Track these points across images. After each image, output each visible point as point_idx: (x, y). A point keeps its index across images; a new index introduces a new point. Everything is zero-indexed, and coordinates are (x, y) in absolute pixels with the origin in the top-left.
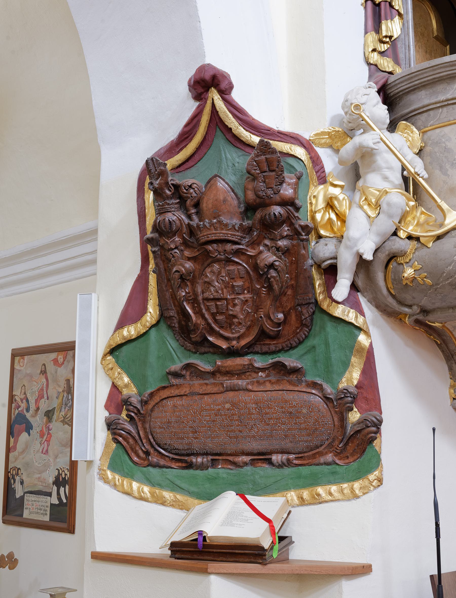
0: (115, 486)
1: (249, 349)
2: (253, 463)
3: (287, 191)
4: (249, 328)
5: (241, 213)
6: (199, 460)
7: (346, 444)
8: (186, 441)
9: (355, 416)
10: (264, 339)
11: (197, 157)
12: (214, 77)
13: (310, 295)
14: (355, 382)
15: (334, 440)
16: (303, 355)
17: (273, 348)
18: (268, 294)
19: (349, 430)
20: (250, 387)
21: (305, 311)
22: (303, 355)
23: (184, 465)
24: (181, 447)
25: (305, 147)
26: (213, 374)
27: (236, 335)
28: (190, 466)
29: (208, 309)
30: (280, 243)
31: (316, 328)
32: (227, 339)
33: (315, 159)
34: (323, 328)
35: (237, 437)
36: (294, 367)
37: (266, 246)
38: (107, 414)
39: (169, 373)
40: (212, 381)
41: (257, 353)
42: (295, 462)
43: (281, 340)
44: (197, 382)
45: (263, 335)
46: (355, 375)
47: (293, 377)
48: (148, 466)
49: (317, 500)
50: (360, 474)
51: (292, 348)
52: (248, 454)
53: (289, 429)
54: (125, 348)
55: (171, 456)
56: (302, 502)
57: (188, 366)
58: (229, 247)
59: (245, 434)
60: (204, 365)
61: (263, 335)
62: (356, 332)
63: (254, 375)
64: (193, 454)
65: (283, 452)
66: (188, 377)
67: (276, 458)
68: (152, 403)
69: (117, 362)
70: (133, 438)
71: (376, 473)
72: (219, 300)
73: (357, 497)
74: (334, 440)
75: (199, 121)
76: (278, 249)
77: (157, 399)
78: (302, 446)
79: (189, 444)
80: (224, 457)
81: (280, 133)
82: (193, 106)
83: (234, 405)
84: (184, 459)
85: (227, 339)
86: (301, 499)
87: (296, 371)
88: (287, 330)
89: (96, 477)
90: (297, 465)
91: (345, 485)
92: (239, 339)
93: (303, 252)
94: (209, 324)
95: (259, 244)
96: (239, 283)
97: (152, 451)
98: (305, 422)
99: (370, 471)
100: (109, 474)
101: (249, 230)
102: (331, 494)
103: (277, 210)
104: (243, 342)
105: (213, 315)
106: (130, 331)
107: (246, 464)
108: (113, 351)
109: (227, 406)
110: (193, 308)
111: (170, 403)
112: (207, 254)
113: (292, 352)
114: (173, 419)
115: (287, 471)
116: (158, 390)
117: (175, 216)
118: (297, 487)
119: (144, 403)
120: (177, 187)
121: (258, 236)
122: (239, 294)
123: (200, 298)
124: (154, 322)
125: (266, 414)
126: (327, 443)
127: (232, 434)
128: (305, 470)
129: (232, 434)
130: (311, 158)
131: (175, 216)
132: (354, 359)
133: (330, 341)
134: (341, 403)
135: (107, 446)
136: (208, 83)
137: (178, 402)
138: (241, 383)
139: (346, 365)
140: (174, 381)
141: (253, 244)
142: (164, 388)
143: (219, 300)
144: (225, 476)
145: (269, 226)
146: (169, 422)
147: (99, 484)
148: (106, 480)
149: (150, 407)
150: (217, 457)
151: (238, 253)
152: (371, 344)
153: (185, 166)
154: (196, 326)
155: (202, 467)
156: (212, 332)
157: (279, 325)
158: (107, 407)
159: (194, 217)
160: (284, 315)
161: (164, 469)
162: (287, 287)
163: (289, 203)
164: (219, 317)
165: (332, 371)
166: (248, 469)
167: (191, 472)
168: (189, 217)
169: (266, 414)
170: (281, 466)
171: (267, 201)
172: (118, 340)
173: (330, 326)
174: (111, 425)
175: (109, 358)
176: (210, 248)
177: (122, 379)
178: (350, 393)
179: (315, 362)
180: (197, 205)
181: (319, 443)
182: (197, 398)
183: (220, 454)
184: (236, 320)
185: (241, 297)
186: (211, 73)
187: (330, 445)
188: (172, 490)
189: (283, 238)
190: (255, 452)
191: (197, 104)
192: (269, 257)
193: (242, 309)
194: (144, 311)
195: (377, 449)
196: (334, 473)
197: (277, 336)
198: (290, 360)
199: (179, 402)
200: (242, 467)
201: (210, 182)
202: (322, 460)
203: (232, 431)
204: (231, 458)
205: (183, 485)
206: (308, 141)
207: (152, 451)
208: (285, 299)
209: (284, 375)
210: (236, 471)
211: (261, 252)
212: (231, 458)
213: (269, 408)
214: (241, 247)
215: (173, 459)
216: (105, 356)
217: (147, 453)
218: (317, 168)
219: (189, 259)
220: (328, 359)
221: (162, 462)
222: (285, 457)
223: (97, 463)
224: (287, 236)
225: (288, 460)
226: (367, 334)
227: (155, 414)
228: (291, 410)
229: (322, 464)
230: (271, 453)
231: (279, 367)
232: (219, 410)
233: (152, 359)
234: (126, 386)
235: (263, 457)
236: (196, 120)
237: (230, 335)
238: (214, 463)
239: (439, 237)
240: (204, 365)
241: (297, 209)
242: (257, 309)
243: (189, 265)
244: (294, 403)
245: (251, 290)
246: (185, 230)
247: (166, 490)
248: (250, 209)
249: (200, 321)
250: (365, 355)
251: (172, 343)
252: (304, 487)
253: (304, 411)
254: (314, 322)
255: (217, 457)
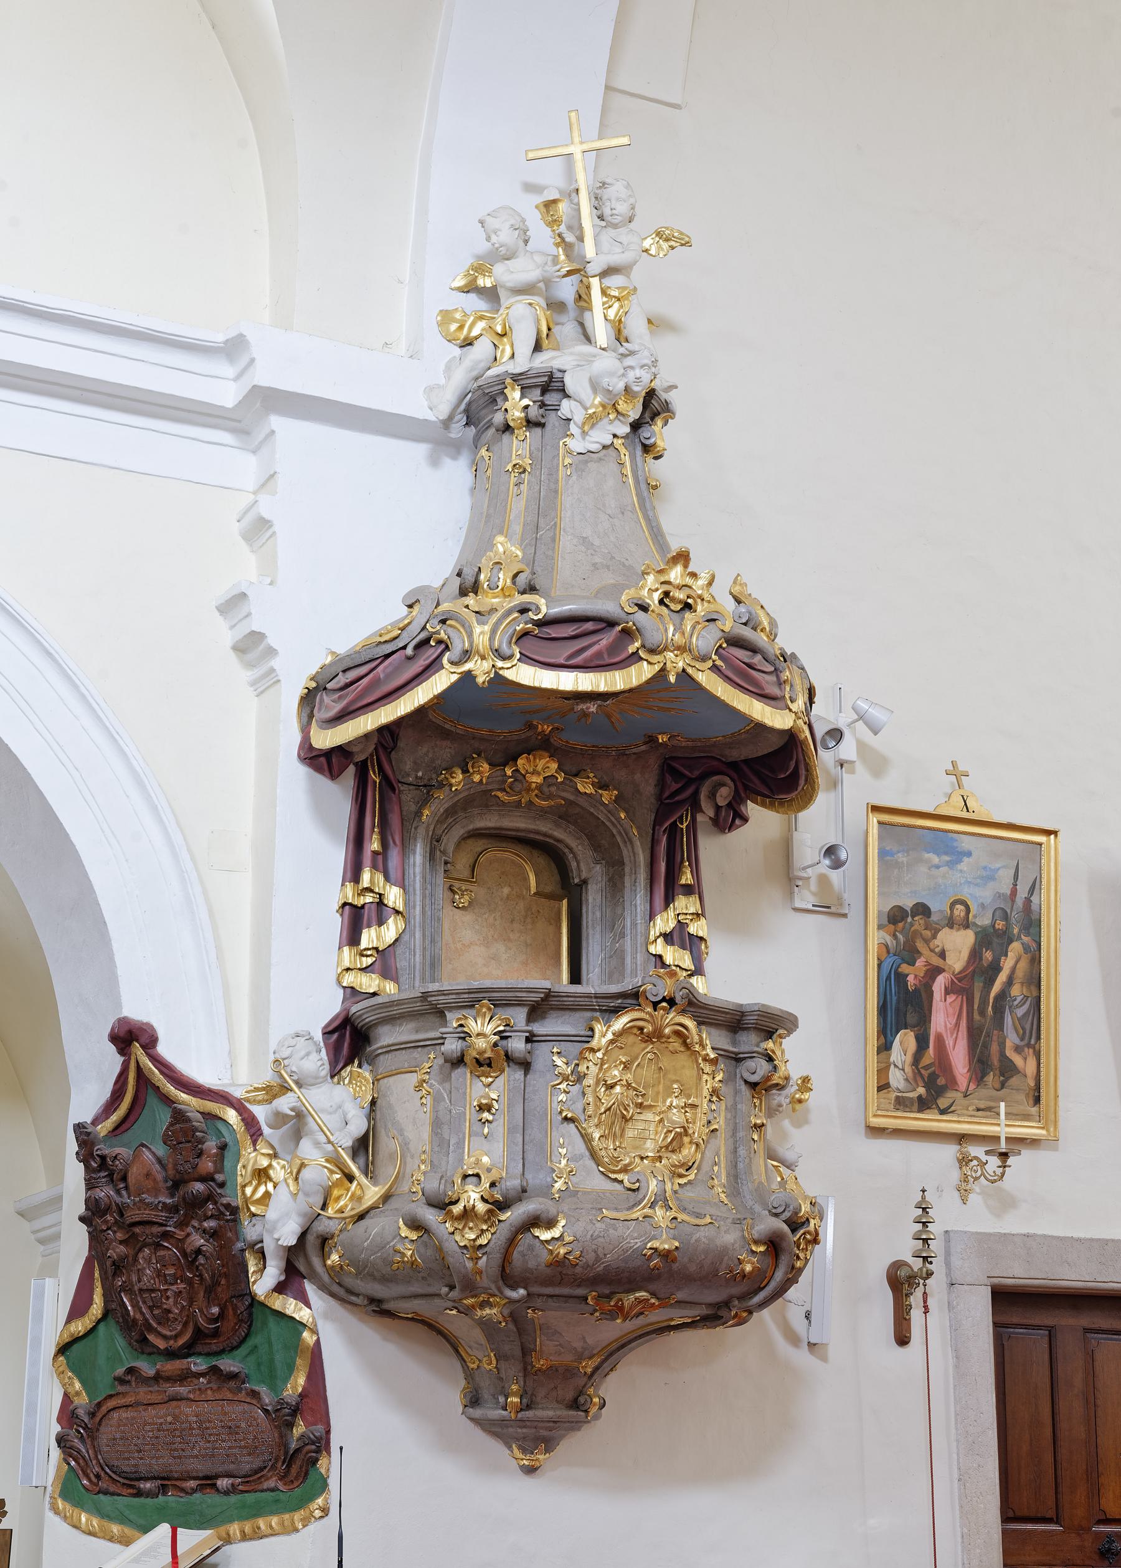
0: (65, 1518)
1: (188, 1351)
2: (201, 1488)
3: (207, 1165)
4: (185, 1324)
5: (168, 1188)
6: (148, 1485)
7: (289, 1466)
8: (133, 1462)
9: (300, 1429)
10: (199, 1340)
11: (132, 1118)
12: (130, 1032)
13: (243, 1286)
14: (300, 1390)
15: (277, 1460)
16: (246, 1356)
17: (214, 1348)
18: (201, 1284)
19: (293, 1446)
20: (191, 1396)
21: (239, 1304)
22: (246, 1356)
23: (135, 1491)
24: (127, 1469)
25: (235, 1109)
26: (158, 1378)
27: (173, 1333)
28: (139, 1494)
29: (144, 1302)
30: (205, 1224)
31: (257, 1324)
32: (165, 1337)
33: (249, 1120)
34: (265, 1323)
35: (180, 1457)
36: (230, 1372)
37: (194, 1227)
38: (59, 1428)
39: (116, 1379)
40: (156, 1388)
41: (200, 1354)
42: (240, 1487)
43: (221, 1339)
44: (143, 1390)
45: (199, 1334)
46: (300, 1380)
47: (232, 1384)
48: (99, 1493)
49: (257, 1535)
50: (303, 1502)
51: (234, 1348)
52: (195, 1478)
53: (230, 1448)
54: (75, 1346)
55: (122, 1480)
56: (245, 1537)
57: (131, 1371)
58: (156, 1230)
59: (187, 1453)
60: (147, 1368)
61: (199, 1334)
62: (301, 1328)
63: (196, 1381)
64: (141, 1479)
65: (228, 1475)
66: (133, 1384)
67: (223, 1483)
68: (99, 1416)
69: (68, 1363)
70: (84, 1458)
71: (320, 1501)
72: (153, 1291)
73: (297, 1530)
74: (277, 1460)
75: (127, 1078)
76: (204, 1231)
77: (104, 1409)
78: (246, 1468)
79: (135, 1466)
80: (174, 1482)
81: (210, 1090)
82: (120, 1059)
83: (176, 1417)
84: (129, 1483)
85: (165, 1337)
86: (243, 1532)
87: (233, 1376)
88: (227, 1326)
89: (47, 1506)
90: (243, 1492)
91: (286, 1516)
92: (176, 1337)
93: (230, 1234)
94: (146, 1320)
95: (187, 1225)
96: (171, 1271)
97: (103, 1474)
98: (244, 1439)
99: (312, 1498)
100: (60, 1503)
101: (173, 1209)
102: (271, 1527)
103: (199, 1187)
104: (180, 1342)
105: (151, 1308)
106: (80, 1327)
107: (194, 1491)
108: (63, 1349)
109: (169, 1419)
110: (131, 1301)
111: (115, 1415)
112: (134, 1236)
113: (236, 1353)
114: (118, 1436)
115: (233, 1499)
116: (105, 1399)
117: (105, 1192)
118: (242, 1518)
119: (92, 1415)
120: (103, 1158)
121: (185, 1215)
122: (172, 1284)
123: (136, 1288)
124: (99, 1316)
125: (207, 1428)
126: (270, 1464)
127: (176, 1454)
128: (250, 1498)
129: (176, 1454)
130: (243, 1120)
131: (105, 1192)
132: (299, 1361)
133: (273, 1338)
134: (285, 1415)
135: (59, 1468)
136: (130, 1037)
137: (125, 1414)
138: (183, 1390)
139: (291, 1368)
140: (120, 1389)
141: (182, 1225)
142: (111, 1396)
143: (153, 1291)
144: (174, 1505)
145: (195, 1204)
146: (114, 1439)
147: (50, 1515)
148: (56, 1512)
149: (98, 1419)
150: (166, 1482)
151: (166, 1235)
152: (318, 1342)
153: (124, 1127)
154: (134, 1320)
155: (149, 1494)
156: (150, 1329)
157: (216, 1320)
158: (59, 1420)
159: (124, 1193)
160: (221, 1309)
161: (116, 1497)
162: (220, 1276)
163: (207, 1178)
164: (156, 1312)
165: (275, 1377)
166: (197, 1495)
167: (142, 1500)
168: (118, 1192)
169: (207, 1428)
170: (227, 1493)
171: (186, 1177)
172: (67, 1338)
173: (272, 1322)
174: (61, 1440)
175: (61, 1358)
176: (137, 1230)
177: (72, 1384)
178: (287, 1403)
179: (259, 1364)
180: (124, 1179)
181: (261, 1464)
182: (141, 1408)
183: (168, 1479)
184: (171, 1316)
185: (174, 1288)
186: (126, 1028)
187: (273, 1467)
188: (121, 1522)
189: (207, 1218)
190: (201, 1475)
191: (123, 1059)
192: (197, 1240)
193: (176, 1303)
194: (90, 1302)
195: (323, 1471)
196: (277, 1501)
197: (216, 1333)
198: (228, 1364)
199: (124, 1415)
200: (191, 1494)
201: (137, 1154)
202: (265, 1485)
203: (175, 1450)
204: (178, 1483)
205: (131, 1517)
206: (239, 1100)
207: (103, 1474)
208: (220, 1289)
209: (224, 1381)
210: (185, 1499)
211: (188, 1235)
212: (178, 1483)
213: (210, 1422)
214: (168, 1229)
215: (124, 1484)
216: (56, 1356)
217: (98, 1476)
218: (253, 1131)
219: (121, 1242)
220: (272, 1361)
221: (112, 1488)
222: (231, 1481)
223: (49, 1489)
224: (212, 1216)
225: (233, 1485)
226: (314, 1331)
227: (102, 1429)
228: (230, 1424)
229: (266, 1490)
230: (217, 1477)
231: (214, 1370)
232: (161, 1424)
233: (101, 1361)
234: (78, 1394)
235: (208, 1482)
236: (122, 1079)
237: (168, 1333)
238: (164, 1489)
239: (361, 1217)
240: (147, 1368)
241: (222, 1185)
242: (191, 1301)
243: (122, 1249)
244: (234, 1416)
245: (184, 1279)
246: (114, 1207)
247: (115, 1523)
248: (177, 1184)
249: (138, 1316)
250: (309, 1355)
251: (120, 1342)
252: (247, 1518)
253: (243, 1425)
254: (255, 1316)
255: (166, 1482)
